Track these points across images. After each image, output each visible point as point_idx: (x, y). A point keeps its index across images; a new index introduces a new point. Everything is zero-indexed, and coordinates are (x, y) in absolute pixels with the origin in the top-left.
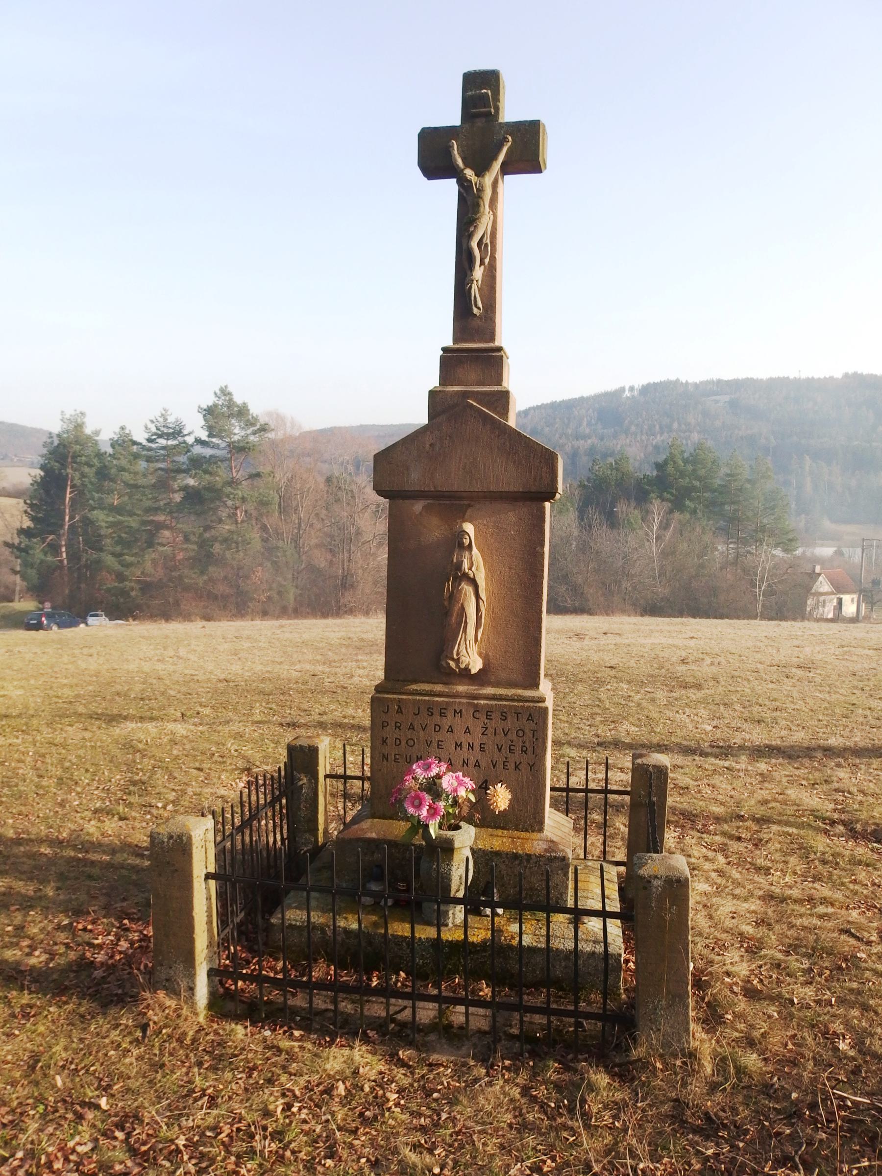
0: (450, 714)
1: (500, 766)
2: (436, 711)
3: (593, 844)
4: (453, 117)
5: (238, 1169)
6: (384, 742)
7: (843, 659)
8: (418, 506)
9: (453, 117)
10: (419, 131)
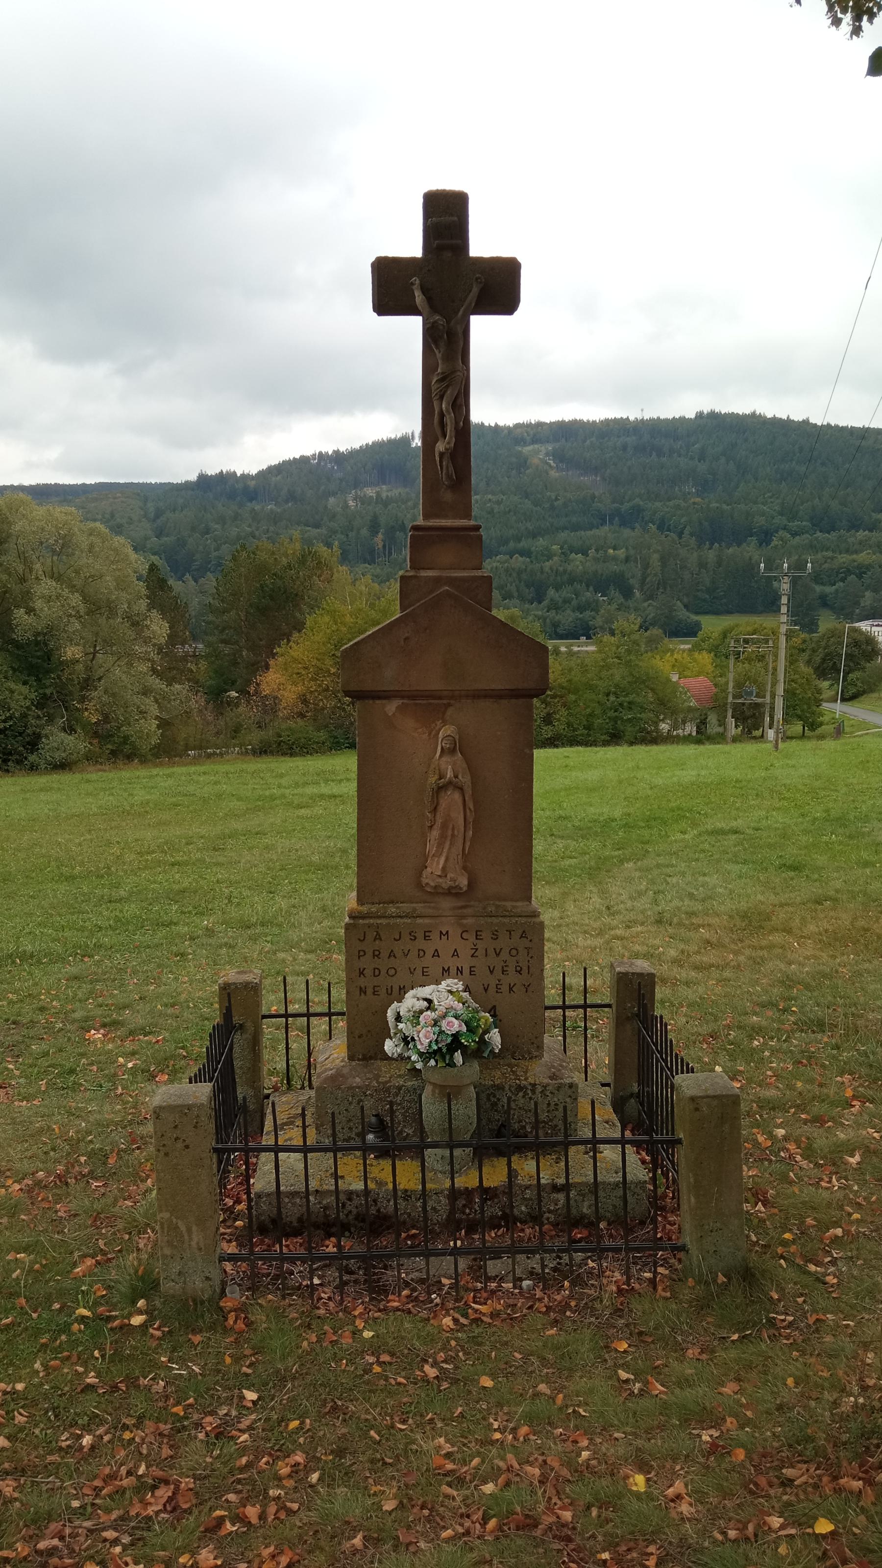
0: (435, 935)
1: (492, 990)
2: (420, 935)
5: (545, 603)
6: (361, 973)
8: (392, 707)
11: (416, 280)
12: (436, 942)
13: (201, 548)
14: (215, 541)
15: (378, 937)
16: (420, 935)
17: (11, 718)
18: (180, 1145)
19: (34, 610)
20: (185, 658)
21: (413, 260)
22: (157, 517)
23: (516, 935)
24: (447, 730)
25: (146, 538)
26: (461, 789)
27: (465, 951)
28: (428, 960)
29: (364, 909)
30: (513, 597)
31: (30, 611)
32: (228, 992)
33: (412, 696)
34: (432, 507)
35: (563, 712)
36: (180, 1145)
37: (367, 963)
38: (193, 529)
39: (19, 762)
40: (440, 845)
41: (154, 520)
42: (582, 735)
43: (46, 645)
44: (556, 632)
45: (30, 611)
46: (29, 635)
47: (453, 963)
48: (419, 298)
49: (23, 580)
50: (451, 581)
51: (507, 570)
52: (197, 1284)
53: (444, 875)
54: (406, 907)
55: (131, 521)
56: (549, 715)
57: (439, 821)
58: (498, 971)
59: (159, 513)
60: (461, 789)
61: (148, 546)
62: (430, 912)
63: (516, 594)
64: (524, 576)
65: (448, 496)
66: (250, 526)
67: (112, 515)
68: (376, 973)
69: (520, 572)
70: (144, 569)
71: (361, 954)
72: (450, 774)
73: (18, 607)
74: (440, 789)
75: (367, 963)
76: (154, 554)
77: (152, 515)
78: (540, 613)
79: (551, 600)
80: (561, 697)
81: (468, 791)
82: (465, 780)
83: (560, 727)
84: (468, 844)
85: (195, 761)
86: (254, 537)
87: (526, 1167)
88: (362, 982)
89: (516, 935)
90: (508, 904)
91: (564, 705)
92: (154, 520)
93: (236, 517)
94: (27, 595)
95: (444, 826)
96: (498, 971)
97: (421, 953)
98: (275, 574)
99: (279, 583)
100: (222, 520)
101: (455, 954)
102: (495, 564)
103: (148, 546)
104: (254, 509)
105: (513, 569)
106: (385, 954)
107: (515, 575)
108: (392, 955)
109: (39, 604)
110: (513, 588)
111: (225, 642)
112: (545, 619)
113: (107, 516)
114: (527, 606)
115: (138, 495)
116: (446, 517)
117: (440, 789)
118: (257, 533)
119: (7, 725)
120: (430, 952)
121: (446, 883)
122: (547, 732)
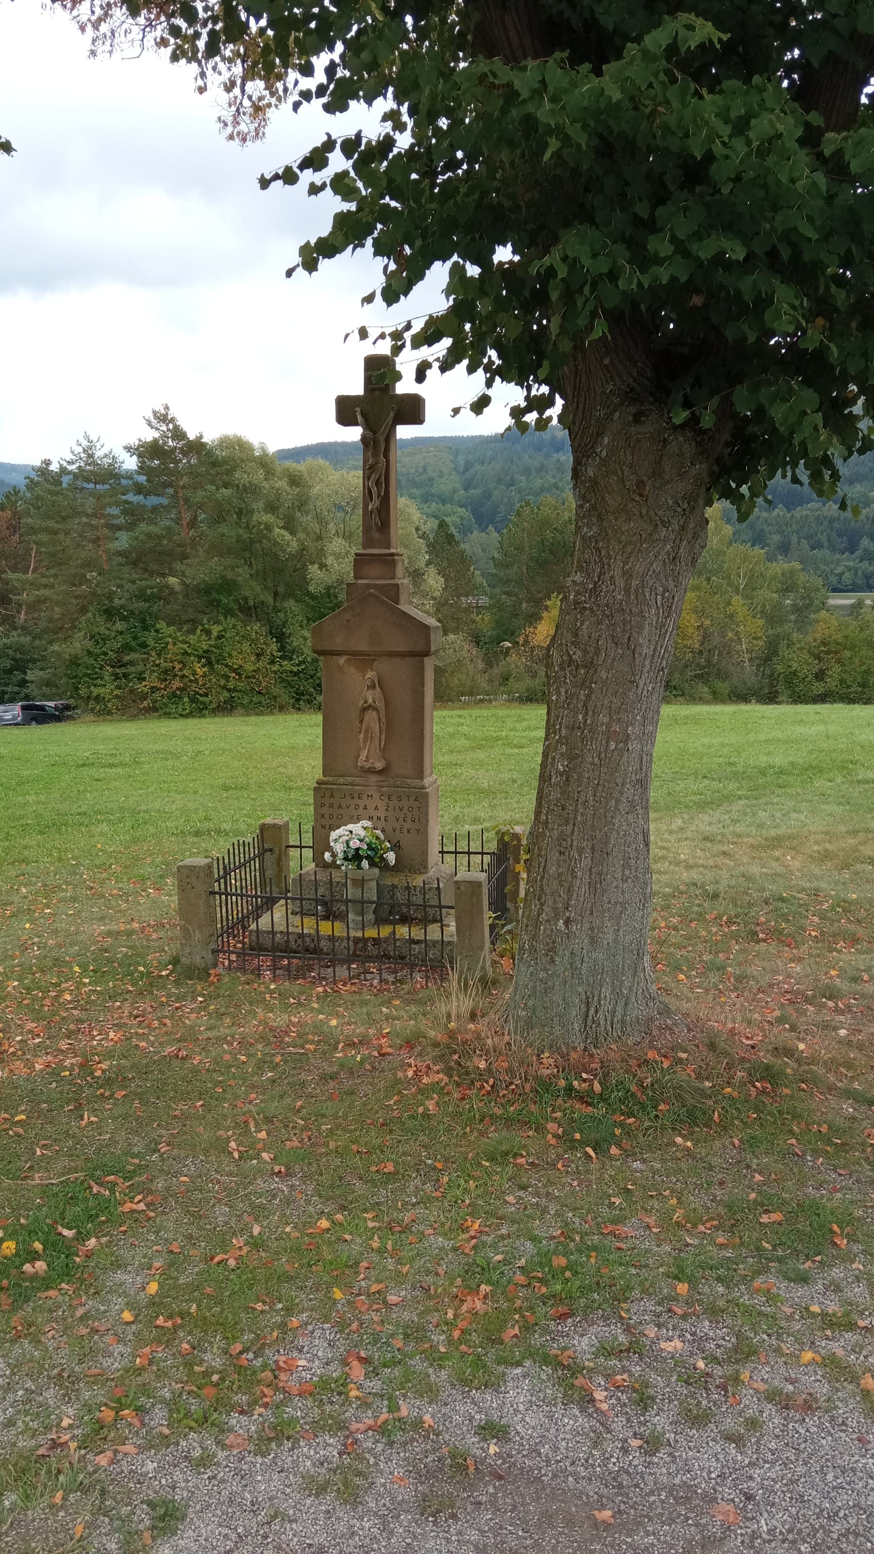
0: (365, 797)
1: (398, 830)
2: (356, 796)
3: (461, 864)
4: (357, 388)
5: (858, 553)
6: (323, 816)
7: (671, 608)
8: (342, 660)
9: (357, 388)
10: (330, 162)
11: (358, 409)
12: (365, 801)
13: (505, 499)
14: (519, 492)
15: (332, 796)
16: (356, 796)
17: (304, 662)
18: (190, 886)
19: (326, 566)
20: (469, 609)
21: (358, 397)
22: (466, 469)
23: (412, 799)
24: (370, 674)
25: (455, 491)
26: (376, 709)
27: (382, 806)
28: (361, 811)
29: (325, 779)
30: (823, 547)
31: (322, 566)
32: (263, 828)
33: (354, 654)
34: (368, 542)
35: (837, 668)
36: (190, 886)
37: (326, 810)
38: (499, 481)
39: (309, 702)
40: (365, 742)
41: (464, 473)
42: (856, 692)
43: (336, 597)
44: (867, 583)
45: (322, 566)
46: (321, 588)
47: (375, 814)
48: (360, 419)
49: (319, 538)
50: (376, 586)
51: (817, 519)
52: (197, 960)
53: (367, 761)
54: (350, 779)
55: (441, 475)
56: (822, 672)
57: (364, 728)
58: (401, 820)
59: (468, 466)
60: (376, 709)
61: (456, 499)
62: (363, 782)
63: (826, 544)
64: (836, 525)
65: (377, 536)
66: (554, 477)
67: (425, 469)
68: (331, 817)
69: (831, 521)
70: (431, 525)
71: (322, 805)
72: (370, 701)
73: (312, 563)
74: (364, 709)
75: (326, 810)
76: (461, 506)
77: (461, 469)
78: (851, 564)
79: (865, 550)
80: (836, 653)
81: (383, 712)
82: (380, 704)
83: (832, 683)
84: (383, 743)
85: (465, 706)
86: (557, 488)
87: (403, 931)
88: (323, 822)
89: (412, 799)
90: (409, 781)
91: (839, 661)
92: (464, 473)
93: (542, 469)
94: (321, 552)
95: (367, 731)
96: (401, 820)
97: (357, 807)
98: (555, 529)
99: (560, 537)
100: (527, 472)
101: (376, 808)
102: (805, 513)
103: (456, 499)
104: (559, 460)
105: (825, 518)
106: (336, 806)
107: (825, 523)
108: (340, 807)
109: (330, 560)
110: (824, 539)
111: (508, 594)
112: (856, 570)
113: (420, 470)
114: (837, 556)
115: (450, 448)
116: (375, 548)
117: (364, 709)
118: (560, 484)
119: (300, 668)
120: (362, 807)
121: (367, 765)
122: (818, 688)
